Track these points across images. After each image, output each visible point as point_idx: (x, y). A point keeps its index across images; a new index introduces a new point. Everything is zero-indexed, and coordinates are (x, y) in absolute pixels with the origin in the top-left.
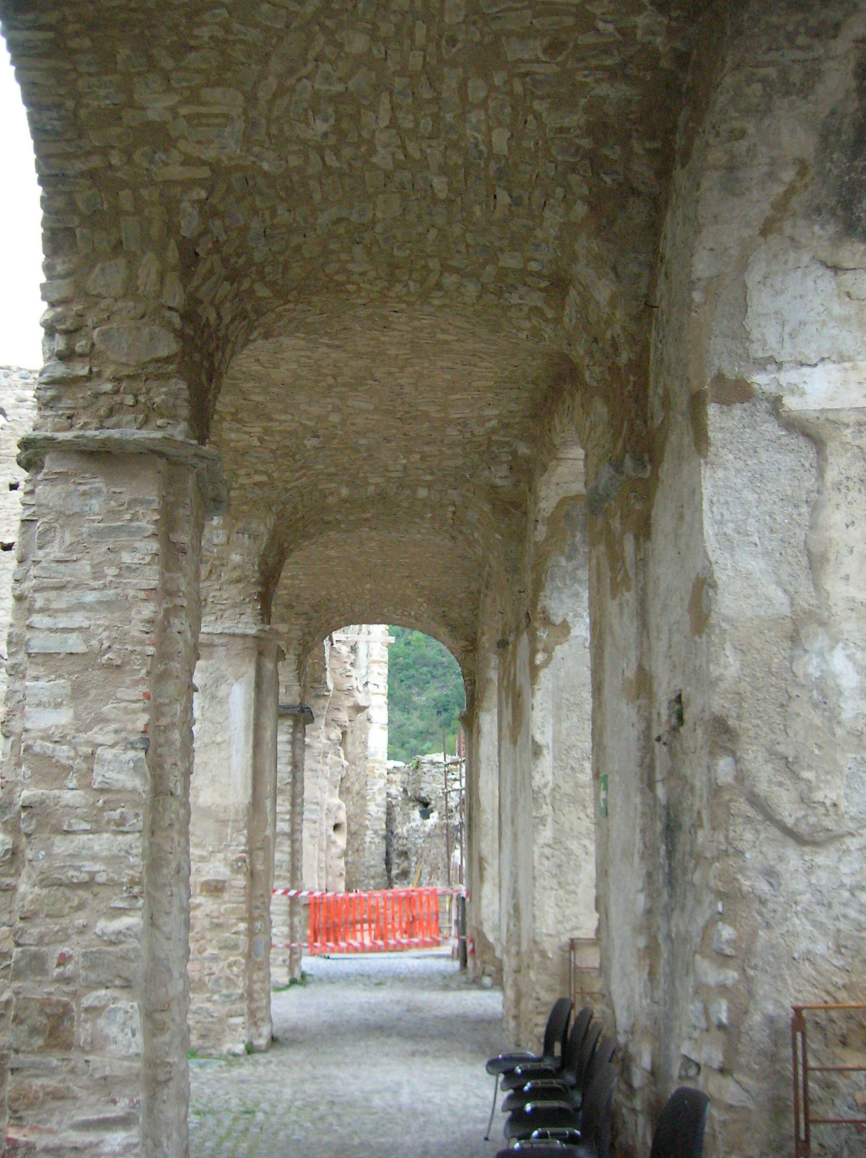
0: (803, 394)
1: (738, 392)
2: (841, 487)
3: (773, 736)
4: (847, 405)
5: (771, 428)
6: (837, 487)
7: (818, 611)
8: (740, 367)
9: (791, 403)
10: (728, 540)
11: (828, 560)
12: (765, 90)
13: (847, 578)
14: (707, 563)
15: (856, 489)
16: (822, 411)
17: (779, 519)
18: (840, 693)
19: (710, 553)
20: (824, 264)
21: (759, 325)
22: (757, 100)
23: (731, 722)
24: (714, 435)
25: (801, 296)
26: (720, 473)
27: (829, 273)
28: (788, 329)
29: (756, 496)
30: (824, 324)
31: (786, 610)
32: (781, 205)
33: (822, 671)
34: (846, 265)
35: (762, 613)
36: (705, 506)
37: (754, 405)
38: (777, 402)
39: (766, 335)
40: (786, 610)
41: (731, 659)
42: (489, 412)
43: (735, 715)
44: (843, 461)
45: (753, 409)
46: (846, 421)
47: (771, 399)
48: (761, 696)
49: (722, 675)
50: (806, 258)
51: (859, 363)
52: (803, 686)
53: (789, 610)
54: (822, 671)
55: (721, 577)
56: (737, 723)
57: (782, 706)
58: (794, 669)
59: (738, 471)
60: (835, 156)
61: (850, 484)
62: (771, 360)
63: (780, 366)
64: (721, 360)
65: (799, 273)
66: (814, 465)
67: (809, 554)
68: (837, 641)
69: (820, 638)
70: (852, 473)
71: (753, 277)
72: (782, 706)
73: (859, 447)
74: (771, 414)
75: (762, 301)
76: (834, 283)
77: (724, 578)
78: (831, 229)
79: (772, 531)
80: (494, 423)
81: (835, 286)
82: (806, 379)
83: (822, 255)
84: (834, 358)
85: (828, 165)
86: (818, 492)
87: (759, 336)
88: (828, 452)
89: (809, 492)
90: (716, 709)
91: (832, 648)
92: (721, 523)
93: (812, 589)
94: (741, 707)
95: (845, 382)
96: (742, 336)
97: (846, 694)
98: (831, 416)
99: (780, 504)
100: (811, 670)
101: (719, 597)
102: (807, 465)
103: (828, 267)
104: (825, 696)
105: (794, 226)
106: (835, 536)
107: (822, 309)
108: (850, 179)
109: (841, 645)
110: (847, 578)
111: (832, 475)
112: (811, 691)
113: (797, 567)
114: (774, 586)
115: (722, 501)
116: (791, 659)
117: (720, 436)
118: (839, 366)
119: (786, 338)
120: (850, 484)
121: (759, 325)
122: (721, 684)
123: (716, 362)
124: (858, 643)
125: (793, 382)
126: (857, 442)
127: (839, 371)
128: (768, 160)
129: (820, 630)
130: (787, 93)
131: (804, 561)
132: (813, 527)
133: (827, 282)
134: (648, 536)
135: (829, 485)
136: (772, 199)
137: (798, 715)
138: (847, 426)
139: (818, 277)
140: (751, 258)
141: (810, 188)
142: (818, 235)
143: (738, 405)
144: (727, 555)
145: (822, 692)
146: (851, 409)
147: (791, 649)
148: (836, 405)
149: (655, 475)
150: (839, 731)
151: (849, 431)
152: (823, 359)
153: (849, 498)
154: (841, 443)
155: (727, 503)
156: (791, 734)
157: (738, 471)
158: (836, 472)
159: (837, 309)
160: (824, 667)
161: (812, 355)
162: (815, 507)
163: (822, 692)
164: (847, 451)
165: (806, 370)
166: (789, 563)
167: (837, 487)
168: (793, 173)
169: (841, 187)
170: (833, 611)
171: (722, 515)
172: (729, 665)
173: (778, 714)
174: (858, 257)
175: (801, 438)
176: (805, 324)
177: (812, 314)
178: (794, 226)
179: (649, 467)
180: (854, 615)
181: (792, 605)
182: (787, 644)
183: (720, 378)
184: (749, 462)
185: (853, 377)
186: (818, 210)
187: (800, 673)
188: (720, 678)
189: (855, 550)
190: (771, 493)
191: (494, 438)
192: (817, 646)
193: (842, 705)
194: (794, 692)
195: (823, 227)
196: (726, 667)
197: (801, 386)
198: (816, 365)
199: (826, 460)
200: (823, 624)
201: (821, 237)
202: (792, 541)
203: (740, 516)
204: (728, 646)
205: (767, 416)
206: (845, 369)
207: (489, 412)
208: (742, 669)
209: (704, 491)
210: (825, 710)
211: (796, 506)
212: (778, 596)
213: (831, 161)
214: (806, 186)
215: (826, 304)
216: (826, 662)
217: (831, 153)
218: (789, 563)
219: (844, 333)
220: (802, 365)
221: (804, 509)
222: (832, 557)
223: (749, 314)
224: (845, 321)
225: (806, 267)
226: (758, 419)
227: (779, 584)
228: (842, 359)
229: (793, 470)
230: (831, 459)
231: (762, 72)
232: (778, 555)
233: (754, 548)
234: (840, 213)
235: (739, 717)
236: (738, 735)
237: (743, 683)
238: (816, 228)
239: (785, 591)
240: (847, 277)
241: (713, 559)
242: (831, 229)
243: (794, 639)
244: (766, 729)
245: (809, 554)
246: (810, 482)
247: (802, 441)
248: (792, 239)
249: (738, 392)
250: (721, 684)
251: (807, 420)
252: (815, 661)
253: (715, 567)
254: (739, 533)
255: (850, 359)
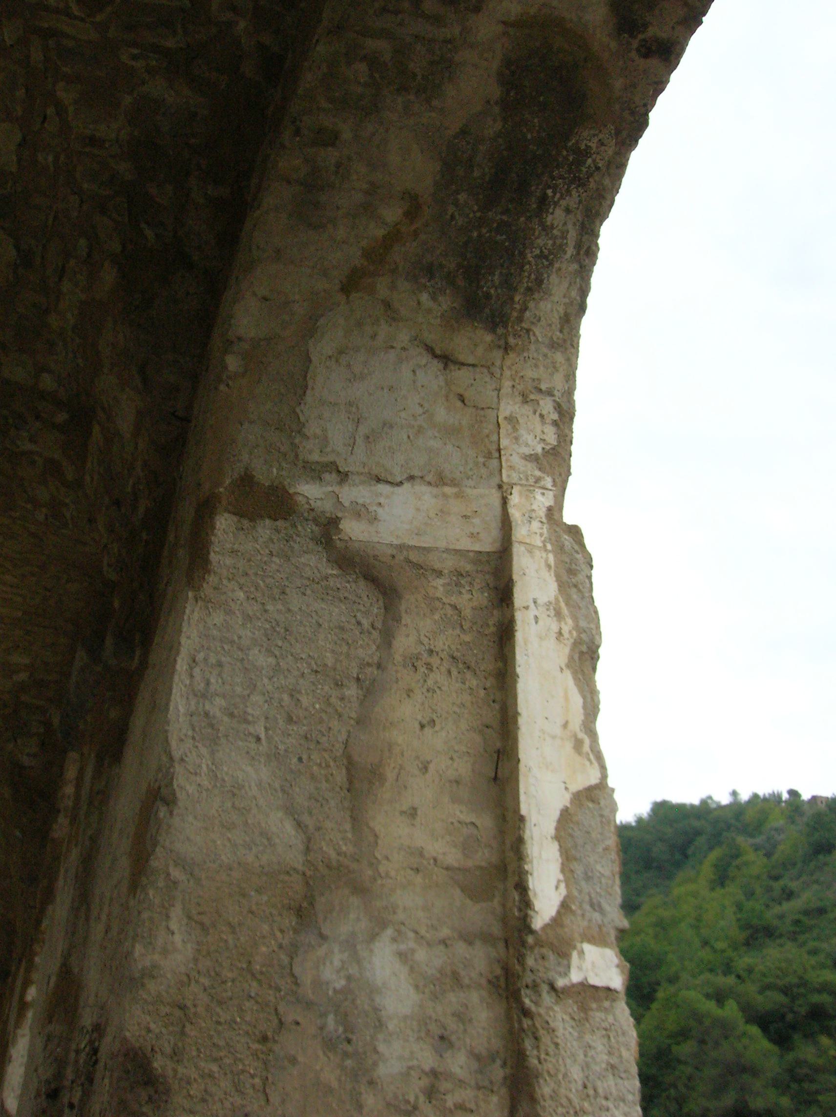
0: (374, 519)
1: (271, 504)
2: (418, 664)
3: (238, 1101)
4: (442, 544)
5: (314, 562)
6: (412, 662)
7: (354, 866)
8: (280, 468)
9: (353, 530)
10: (212, 726)
11: (382, 779)
12: (371, 76)
13: (412, 813)
14: (165, 759)
15: (443, 669)
16: (401, 547)
17: (305, 701)
18: (380, 1025)
19: (174, 743)
20: (430, 350)
21: (320, 417)
22: (360, 90)
23: (158, 1063)
24: (219, 558)
25: (391, 388)
26: (218, 618)
27: (436, 365)
28: (363, 430)
29: (271, 660)
30: (420, 430)
31: (295, 858)
32: (377, 256)
33: (349, 978)
34: (462, 358)
35: (250, 858)
36: (181, 665)
37: (294, 526)
38: (331, 524)
39: (329, 430)
40: (295, 858)
41: (177, 938)
42: (17, 659)
43: (168, 1050)
44: (427, 625)
45: (291, 531)
46: (437, 566)
47: (323, 520)
48: (224, 1017)
49: (155, 966)
50: (404, 337)
51: (469, 491)
52: (309, 1005)
53: (301, 858)
54: (349, 978)
55: (185, 786)
56: (170, 1065)
57: (264, 1039)
58: (297, 970)
59: (248, 618)
60: (462, 197)
61: (435, 661)
62: (333, 467)
63: (344, 477)
64: (251, 451)
65: (392, 355)
66: (379, 625)
67: (350, 765)
68: (383, 924)
69: (352, 916)
70: (441, 643)
71: (322, 348)
72: (264, 1039)
73: (455, 607)
74: (318, 542)
75: (328, 383)
76: (441, 378)
77: (191, 789)
78: (446, 302)
79: (290, 720)
80: (23, 676)
81: (443, 384)
82: (382, 500)
83: (429, 337)
84: (429, 478)
85: (451, 209)
86: (379, 666)
87: (318, 431)
88: (403, 608)
89: (364, 665)
90: (133, 1032)
91: (373, 937)
92: (204, 696)
93: (348, 826)
94: (183, 1033)
95: (442, 513)
96: (292, 427)
97: (391, 1026)
98: (413, 557)
99: (312, 677)
100: (328, 974)
101: (176, 821)
102: (366, 623)
103: (435, 356)
104: (349, 1029)
105: (393, 287)
106: (400, 740)
107: (420, 411)
108: (480, 236)
109: (389, 932)
110: (412, 813)
111: (405, 642)
112: (324, 1015)
113: (324, 785)
114: (280, 814)
115: (213, 660)
116: (293, 950)
117: (229, 561)
118: (435, 490)
119: (360, 441)
120: (435, 661)
121: (320, 417)
122: (151, 985)
123: (245, 457)
124: (423, 932)
125: (360, 501)
126: (453, 599)
127: (436, 497)
128: (365, 186)
129: (355, 901)
130: (403, 89)
131: (340, 776)
132: (361, 722)
133: (431, 376)
134: (117, 756)
135: (398, 658)
136: (364, 243)
137: (293, 1061)
138: (439, 574)
139: (420, 367)
140: (321, 322)
141: (423, 237)
142: (429, 306)
143: (268, 522)
144: (204, 751)
145: (344, 1019)
146: (447, 550)
147: (296, 931)
148: (425, 542)
149: (144, 664)
150: (370, 1100)
151: (440, 581)
152: (411, 478)
153: (430, 682)
154: (426, 597)
155: (220, 664)
156: (275, 1098)
157: (248, 618)
158: (412, 639)
159: (441, 414)
160: (353, 970)
161: (397, 470)
162: (370, 691)
163: (344, 1019)
164: (433, 610)
165: (382, 488)
166: (313, 777)
167: (412, 662)
168: (400, 212)
169: (466, 244)
170: (382, 869)
171: (208, 683)
172: (171, 949)
173: (255, 1055)
174: (480, 350)
175: (362, 583)
176: (391, 427)
177: (403, 414)
178: (393, 287)
179: (138, 653)
180: (419, 879)
181: (308, 850)
182: (289, 920)
183: (247, 480)
184: (269, 607)
185: (457, 507)
186: (430, 271)
187: (307, 980)
188: (151, 973)
189: (432, 767)
190: (297, 659)
191: (24, 698)
192: (344, 929)
193: (382, 1047)
194: (291, 1014)
195: (434, 298)
196: (165, 952)
197: (373, 508)
198: (400, 484)
199: (398, 620)
200: (360, 890)
201: (429, 311)
202: (324, 740)
203: (239, 690)
204: (177, 912)
205: (312, 545)
206: (445, 496)
207: (17, 659)
208: (196, 960)
209: (183, 640)
210: (346, 1055)
211: (339, 685)
212: (285, 831)
213: (456, 204)
214: (416, 234)
215: (426, 405)
216: (359, 962)
217: (457, 192)
218: (313, 777)
219: (449, 447)
220: (379, 480)
221: (352, 691)
222: (390, 775)
223: (308, 398)
224: (450, 432)
225: (404, 349)
226: (296, 546)
227: (290, 810)
228: (441, 480)
229: (342, 629)
230: (406, 619)
231: (372, 44)
232: (295, 760)
233: (253, 745)
234: (461, 282)
235: (176, 1055)
236: (167, 1091)
237: (194, 987)
238: (424, 297)
239: (299, 825)
240: (463, 376)
241: (176, 754)
242: (446, 302)
243: (304, 913)
244: (225, 1084)
245: (350, 765)
246: (367, 650)
247: (363, 588)
248: (387, 305)
249: (271, 504)
250: (151, 985)
251: (375, 557)
252: (338, 958)
253: (178, 769)
254: (232, 715)
255: (454, 483)
